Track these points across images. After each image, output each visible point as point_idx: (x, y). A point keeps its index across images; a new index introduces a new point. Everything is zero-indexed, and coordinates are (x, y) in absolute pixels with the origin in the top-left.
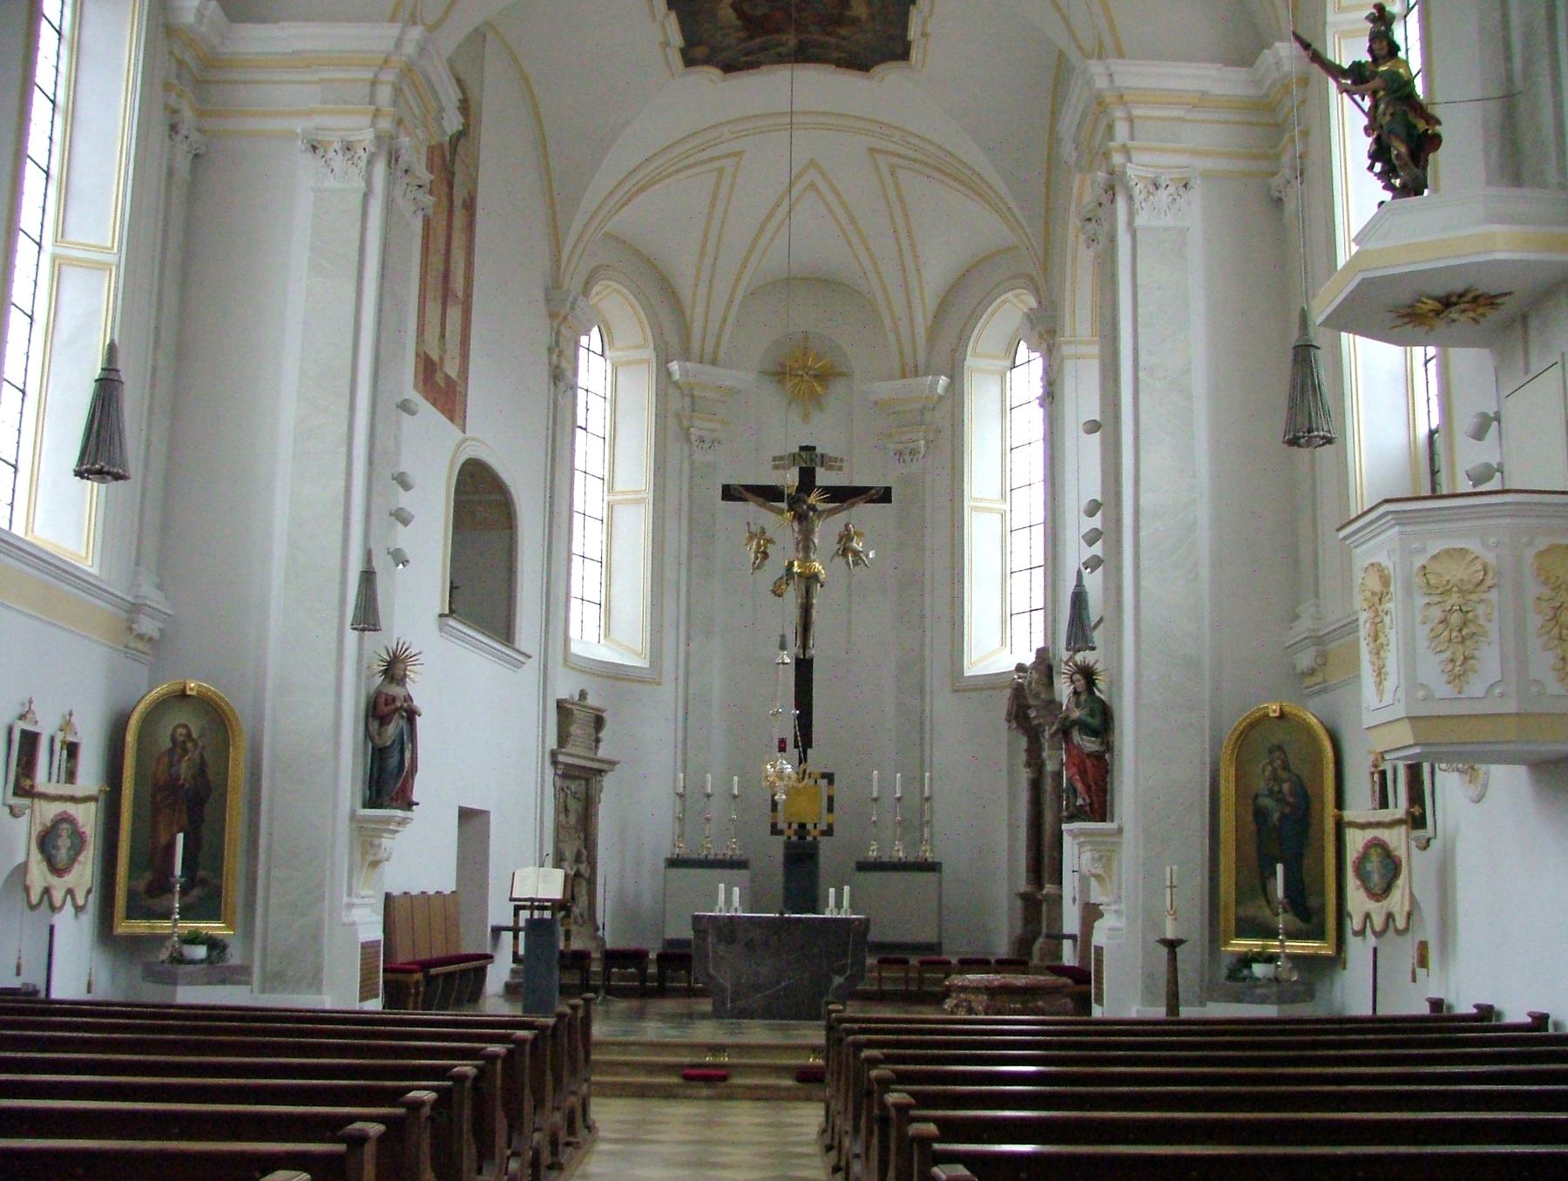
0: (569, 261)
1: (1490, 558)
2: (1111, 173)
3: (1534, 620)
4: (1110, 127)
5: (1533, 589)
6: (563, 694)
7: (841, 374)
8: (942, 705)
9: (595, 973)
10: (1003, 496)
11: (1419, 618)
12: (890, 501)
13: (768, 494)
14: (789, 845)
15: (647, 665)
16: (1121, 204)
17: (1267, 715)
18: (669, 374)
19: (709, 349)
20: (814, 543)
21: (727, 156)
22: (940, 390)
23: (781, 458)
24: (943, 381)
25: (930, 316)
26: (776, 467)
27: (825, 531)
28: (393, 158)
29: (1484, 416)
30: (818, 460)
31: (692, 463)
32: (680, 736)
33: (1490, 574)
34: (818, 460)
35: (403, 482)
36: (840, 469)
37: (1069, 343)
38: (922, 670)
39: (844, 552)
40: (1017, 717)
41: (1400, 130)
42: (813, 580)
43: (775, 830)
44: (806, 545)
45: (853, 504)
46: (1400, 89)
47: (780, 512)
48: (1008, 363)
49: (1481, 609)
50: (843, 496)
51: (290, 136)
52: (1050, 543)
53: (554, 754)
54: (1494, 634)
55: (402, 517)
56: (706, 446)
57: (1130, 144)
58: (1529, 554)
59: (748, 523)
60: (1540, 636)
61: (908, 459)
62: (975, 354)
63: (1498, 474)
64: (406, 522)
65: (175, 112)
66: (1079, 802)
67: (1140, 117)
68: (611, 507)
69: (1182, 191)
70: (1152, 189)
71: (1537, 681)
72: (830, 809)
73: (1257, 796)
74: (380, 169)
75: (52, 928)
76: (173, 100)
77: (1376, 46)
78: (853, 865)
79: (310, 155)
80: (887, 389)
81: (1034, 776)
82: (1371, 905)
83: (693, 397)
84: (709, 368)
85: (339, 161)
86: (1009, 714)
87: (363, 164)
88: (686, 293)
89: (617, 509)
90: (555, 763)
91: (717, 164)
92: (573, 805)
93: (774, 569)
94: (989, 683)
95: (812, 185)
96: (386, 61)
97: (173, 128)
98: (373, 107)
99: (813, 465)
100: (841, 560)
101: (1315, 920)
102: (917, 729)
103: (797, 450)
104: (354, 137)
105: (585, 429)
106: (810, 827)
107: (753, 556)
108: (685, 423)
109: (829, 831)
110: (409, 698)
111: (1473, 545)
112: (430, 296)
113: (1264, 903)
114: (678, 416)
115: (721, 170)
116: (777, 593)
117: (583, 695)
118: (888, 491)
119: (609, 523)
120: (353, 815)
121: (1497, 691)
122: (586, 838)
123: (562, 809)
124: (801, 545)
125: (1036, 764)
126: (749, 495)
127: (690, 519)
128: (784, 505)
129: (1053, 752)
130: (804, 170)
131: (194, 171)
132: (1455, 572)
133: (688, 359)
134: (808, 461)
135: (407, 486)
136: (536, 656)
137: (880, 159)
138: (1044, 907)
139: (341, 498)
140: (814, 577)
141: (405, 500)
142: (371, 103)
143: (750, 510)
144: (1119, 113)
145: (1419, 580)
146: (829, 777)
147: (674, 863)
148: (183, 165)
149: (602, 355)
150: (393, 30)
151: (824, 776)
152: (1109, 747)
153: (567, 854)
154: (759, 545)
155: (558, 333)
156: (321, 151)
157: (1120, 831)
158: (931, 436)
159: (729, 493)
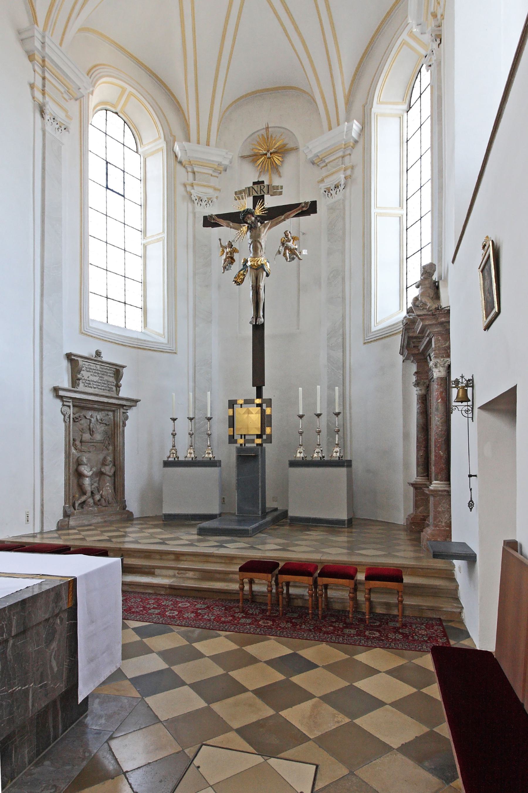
7: (292, 149)
10: (401, 205)
14: (240, 450)
15: (166, 342)
20: (260, 244)
22: (354, 134)
24: (356, 126)
30: (265, 190)
32: (191, 384)
34: (265, 190)
38: (344, 335)
42: (261, 270)
43: (232, 439)
48: (405, 107)
52: (435, 107)
56: (204, 203)
59: (220, 240)
61: (333, 192)
62: (380, 103)
68: (145, 247)
78: (288, 463)
81: (423, 392)
83: (194, 173)
86: (402, 347)
99: (263, 193)
103: (251, 185)
105: (123, 196)
107: (223, 262)
114: (185, 185)
116: (238, 282)
117: (98, 353)
124: (251, 246)
125: (425, 383)
127: (194, 252)
129: (440, 361)
138: (431, 499)
140: (262, 267)
147: (167, 464)
149: (137, 152)
158: (349, 172)
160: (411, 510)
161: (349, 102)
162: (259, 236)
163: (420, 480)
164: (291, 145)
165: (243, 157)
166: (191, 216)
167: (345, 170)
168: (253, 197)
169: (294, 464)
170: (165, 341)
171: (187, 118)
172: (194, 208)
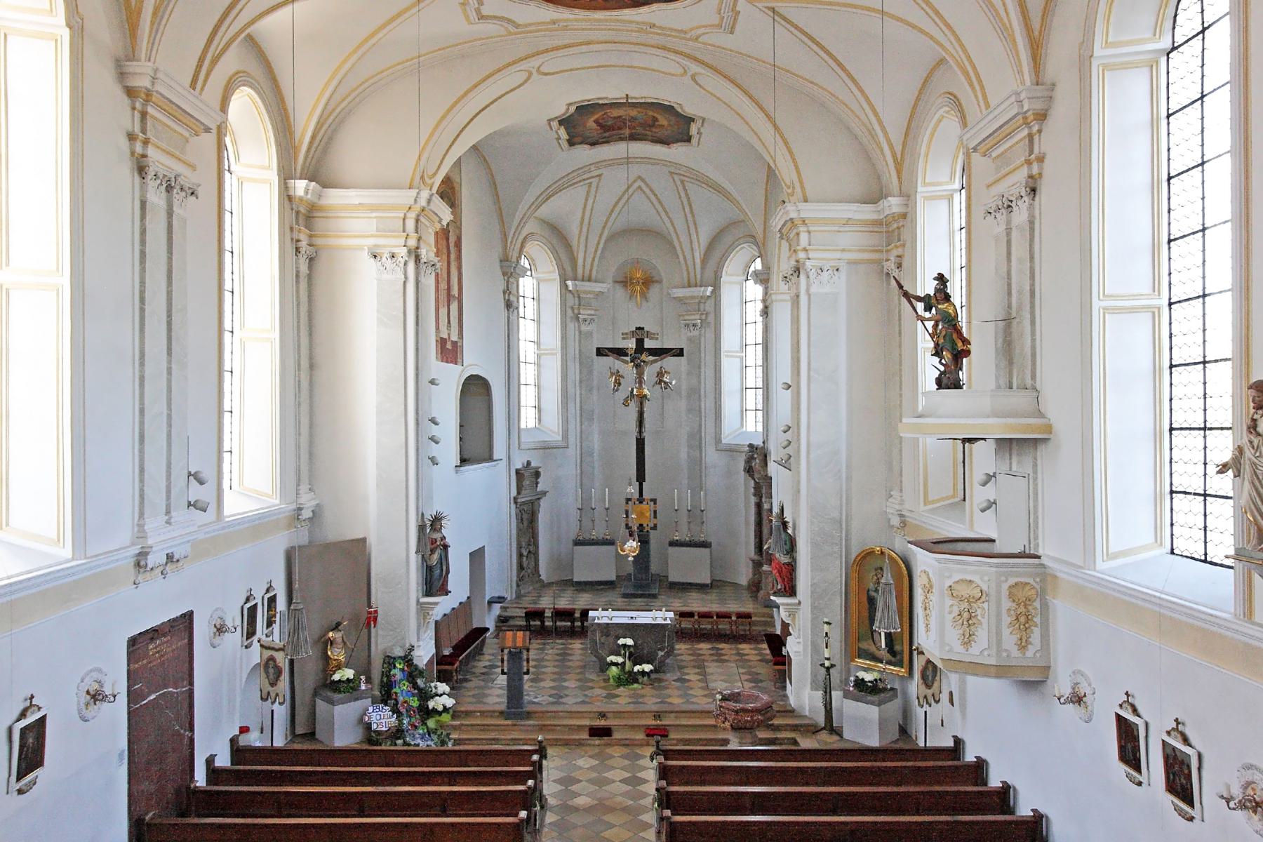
0: (511, 242)
1: (985, 588)
2: (797, 261)
3: (1007, 619)
4: (798, 234)
5: (1007, 604)
6: (519, 466)
8: (711, 456)
9: (548, 617)
11: (947, 610)
12: (683, 356)
13: (620, 353)
16: (802, 277)
17: (874, 552)
18: (567, 286)
19: (587, 273)
21: (593, 177)
22: (708, 294)
23: (627, 334)
24: (710, 289)
25: (702, 253)
26: (624, 339)
27: (650, 373)
28: (418, 259)
29: (988, 475)
31: (580, 332)
33: (984, 595)
34: (645, 335)
35: (434, 421)
36: (657, 339)
37: (775, 294)
39: (661, 381)
40: (748, 472)
41: (948, 346)
44: (640, 380)
45: (664, 358)
46: (951, 322)
47: (626, 362)
48: (745, 278)
49: (979, 612)
50: (660, 353)
51: (361, 248)
53: (515, 498)
54: (984, 621)
55: (434, 440)
56: (587, 323)
57: (808, 248)
58: (1005, 586)
60: (1009, 627)
63: (994, 505)
64: (437, 443)
65: (298, 241)
66: (779, 587)
67: (814, 231)
69: (835, 272)
70: (819, 271)
71: (1006, 650)
72: (655, 517)
73: (868, 591)
74: (411, 266)
75: (272, 711)
76: (296, 236)
77: (937, 295)
79: (372, 260)
80: (680, 293)
82: (270, 689)
83: (579, 297)
84: (588, 283)
85: (389, 262)
87: (402, 265)
88: (574, 243)
89: (542, 357)
90: (516, 503)
91: (589, 181)
92: (525, 516)
93: (623, 393)
94: (731, 450)
95: (640, 187)
96: (410, 208)
97: (298, 250)
98: (405, 234)
100: (658, 386)
101: (898, 657)
102: (697, 466)
104: (396, 250)
106: (645, 525)
108: (576, 311)
109: (655, 528)
110: (443, 538)
111: (976, 579)
112: (441, 306)
113: (871, 640)
114: (572, 308)
115: (591, 183)
116: (626, 404)
118: (682, 350)
119: (538, 364)
120: (418, 601)
121: (986, 653)
122: (533, 533)
123: (520, 520)
126: (610, 353)
127: (580, 364)
128: (628, 359)
130: (635, 181)
131: (310, 267)
132: (965, 591)
133: (575, 280)
134: (640, 334)
135: (436, 424)
136: (504, 460)
137: (675, 177)
139: (404, 445)
140: (645, 396)
141: (435, 431)
142: (404, 231)
143: (610, 361)
144: (802, 229)
145: (947, 593)
146: (654, 501)
148: (304, 268)
150: (414, 192)
151: (652, 500)
152: (794, 560)
153: (523, 544)
154: (616, 379)
155: (508, 282)
156: (378, 258)
157: (800, 603)
159: (600, 352)
160: (751, 576)
161: (704, 262)
162: (643, 373)
163: (756, 557)
164: (656, 278)
165: (616, 282)
166: (577, 333)
167: (702, 314)
168: (637, 339)
169: (673, 544)
170: (560, 438)
171: (575, 254)
172: (579, 327)
